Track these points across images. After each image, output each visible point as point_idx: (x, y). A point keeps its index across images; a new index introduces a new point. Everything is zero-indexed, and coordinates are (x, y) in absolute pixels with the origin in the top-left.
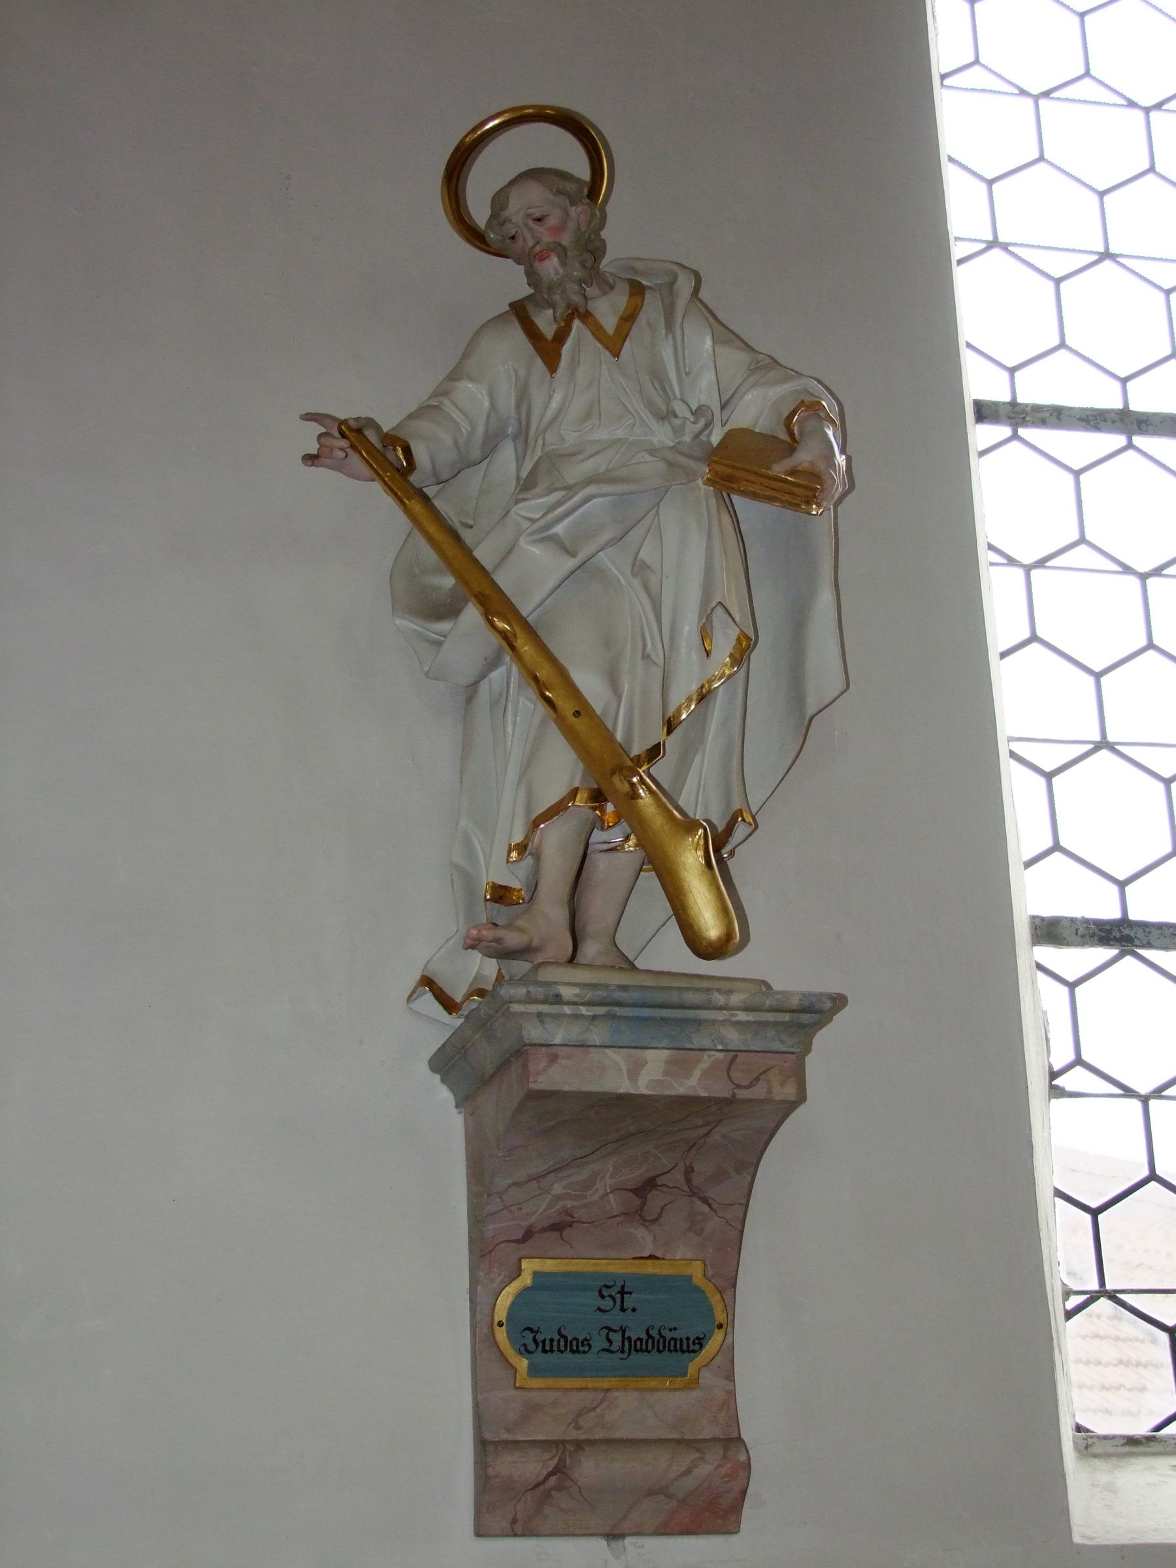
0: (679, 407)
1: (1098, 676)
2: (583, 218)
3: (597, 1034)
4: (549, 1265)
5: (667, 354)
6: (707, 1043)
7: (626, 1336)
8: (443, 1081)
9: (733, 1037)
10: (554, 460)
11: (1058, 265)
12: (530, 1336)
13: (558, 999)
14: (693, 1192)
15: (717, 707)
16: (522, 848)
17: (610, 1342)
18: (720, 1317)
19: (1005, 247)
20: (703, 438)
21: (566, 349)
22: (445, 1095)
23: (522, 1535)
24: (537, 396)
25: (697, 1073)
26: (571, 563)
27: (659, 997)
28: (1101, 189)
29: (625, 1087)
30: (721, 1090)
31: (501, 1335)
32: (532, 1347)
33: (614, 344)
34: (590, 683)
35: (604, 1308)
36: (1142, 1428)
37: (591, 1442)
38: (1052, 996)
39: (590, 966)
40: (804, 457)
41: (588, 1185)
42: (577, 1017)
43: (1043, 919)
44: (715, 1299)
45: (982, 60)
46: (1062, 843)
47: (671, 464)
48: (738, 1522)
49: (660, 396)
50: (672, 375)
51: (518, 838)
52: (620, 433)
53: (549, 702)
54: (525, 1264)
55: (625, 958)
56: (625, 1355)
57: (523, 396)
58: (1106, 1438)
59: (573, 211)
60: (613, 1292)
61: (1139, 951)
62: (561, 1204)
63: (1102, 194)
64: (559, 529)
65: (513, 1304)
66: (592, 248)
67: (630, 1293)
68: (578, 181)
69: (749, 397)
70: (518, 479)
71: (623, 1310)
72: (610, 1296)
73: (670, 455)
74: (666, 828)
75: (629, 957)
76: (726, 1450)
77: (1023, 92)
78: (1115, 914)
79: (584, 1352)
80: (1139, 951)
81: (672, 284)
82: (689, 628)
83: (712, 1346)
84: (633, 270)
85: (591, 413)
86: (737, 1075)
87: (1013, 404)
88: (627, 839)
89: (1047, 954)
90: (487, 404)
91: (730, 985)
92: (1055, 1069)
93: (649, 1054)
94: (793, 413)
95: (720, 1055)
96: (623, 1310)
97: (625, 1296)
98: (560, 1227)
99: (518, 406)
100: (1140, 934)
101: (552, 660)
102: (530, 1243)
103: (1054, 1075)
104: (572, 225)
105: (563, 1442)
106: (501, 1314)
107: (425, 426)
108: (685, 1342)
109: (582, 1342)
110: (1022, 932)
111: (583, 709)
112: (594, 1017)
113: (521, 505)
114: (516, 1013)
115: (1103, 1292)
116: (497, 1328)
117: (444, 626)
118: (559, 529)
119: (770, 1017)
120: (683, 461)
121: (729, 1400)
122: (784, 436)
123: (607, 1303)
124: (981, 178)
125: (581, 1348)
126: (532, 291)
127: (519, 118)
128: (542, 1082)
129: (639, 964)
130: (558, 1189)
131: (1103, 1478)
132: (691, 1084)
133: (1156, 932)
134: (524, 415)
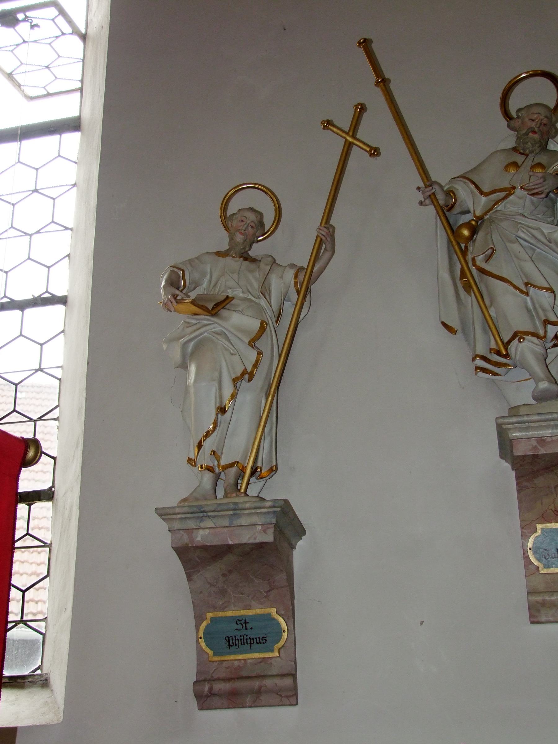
7: (236, 638)
49: (216, 307)
55: (271, 501)
60: (243, 622)
67: (248, 623)
71: (246, 629)
79: (263, 643)
97: (247, 624)
108: (258, 639)
109: (262, 639)
116: (199, 639)
123: (239, 627)
125: (261, 641)
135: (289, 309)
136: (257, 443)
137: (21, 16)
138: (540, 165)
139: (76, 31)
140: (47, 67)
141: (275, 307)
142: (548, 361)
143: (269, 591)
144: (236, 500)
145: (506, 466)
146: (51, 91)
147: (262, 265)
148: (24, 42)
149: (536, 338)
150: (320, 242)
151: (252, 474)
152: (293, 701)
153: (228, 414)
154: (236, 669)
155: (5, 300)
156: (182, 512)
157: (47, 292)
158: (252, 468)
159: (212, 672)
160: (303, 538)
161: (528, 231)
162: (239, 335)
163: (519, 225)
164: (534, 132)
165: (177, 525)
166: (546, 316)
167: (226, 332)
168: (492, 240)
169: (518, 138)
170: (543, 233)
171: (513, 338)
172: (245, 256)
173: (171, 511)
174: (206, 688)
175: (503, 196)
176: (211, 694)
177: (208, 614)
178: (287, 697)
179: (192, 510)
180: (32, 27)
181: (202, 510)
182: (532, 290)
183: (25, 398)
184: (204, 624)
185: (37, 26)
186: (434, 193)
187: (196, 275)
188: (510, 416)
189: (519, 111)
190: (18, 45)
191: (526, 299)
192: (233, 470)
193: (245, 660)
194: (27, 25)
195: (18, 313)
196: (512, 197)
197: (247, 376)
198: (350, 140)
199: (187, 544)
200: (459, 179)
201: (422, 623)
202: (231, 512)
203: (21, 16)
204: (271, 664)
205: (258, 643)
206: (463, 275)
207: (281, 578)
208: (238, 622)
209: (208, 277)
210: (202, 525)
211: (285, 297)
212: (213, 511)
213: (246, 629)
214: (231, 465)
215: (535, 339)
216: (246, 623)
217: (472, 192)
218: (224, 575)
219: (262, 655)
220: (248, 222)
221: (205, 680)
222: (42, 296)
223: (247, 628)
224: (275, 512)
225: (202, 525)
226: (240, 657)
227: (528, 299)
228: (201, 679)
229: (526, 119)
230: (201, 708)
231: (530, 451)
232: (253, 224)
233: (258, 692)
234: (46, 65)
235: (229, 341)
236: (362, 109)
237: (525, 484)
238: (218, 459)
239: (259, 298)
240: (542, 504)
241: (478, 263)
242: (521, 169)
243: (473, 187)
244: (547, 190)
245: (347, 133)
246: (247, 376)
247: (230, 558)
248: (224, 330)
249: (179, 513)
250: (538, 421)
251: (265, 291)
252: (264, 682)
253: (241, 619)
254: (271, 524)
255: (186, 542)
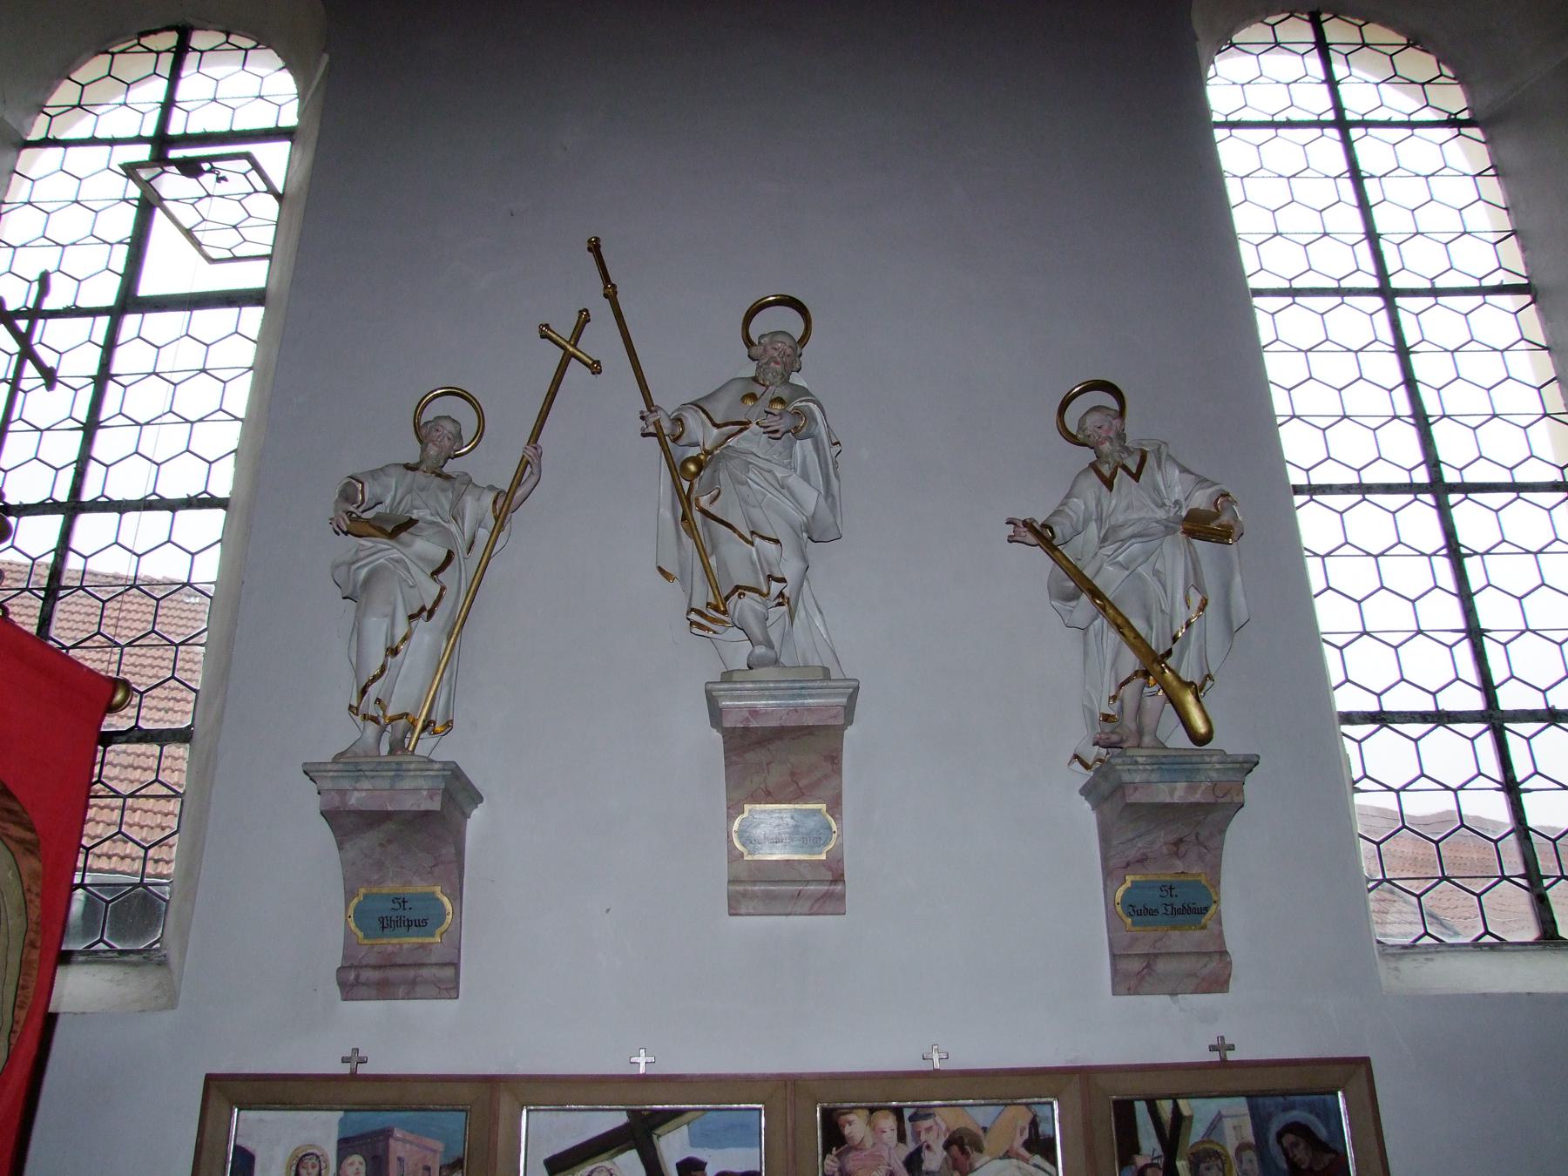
0: (1166, 501)
1: (1359, 602)
2: (1118, 425)
3: (1154, 777)
4: (1138, 878)
5: (1159, 478)
6: (1203, 779)
8: (1086, 799)
9: (1214, 775)
10: (1115, 529)
11: (1323, 423)
12: (1131, 908)
13: (1136, 763)
14: (1200, 844)
15: (1194, 630)
16: (1114, 698)
17: (1166, 910)
18: (1215, 898)
19: (1298, 417)
20: (1179, 513)
21: (1115, 481)
22: (1087, 805)
23: (1134, 994)
24: (1105, 502)
25: (1199, 792)
26: (1127, 573)
27: (1181, 760)
29: (1168, 800)
30: (1211, 799)
31: (1119, 908)
32: (1132, 913)
33: (1136, 477)
34: (1138, 624)
36: (1408, 941)
37: (1161, 954)
38: (1350, 748)
39: (1148, 748)
40: (1225, 519)
41: (1152, 843)
42: (1145, 770)
43: (1344, 713)
44: (1212, 890)
46: (1350, 678)
47: (1166, 527)
48: (1228, 988)
50: (1162, 487)
51: (1112, 694)
52: (1142, 514)
53: (1122, 633)
54: (1127, 877)
57: (1099, 502)
58: (1392, 946)
59: (1114, 422)
61: (1390, 725)
62: (1141, 851)
64: (1120, 558)
65: (1123, 895)
66: (1121, 436)
68: (1115, 410)
69: (1197, 494)
70: (1099, 537)
71: (1171, 896)
73: (1166, 523)
74: (1179, 686)
76: (1221, 956)
77: (1300, 350)
78: (1376, 708)
80: (1390, 725)
81: (1159, 449)
82: (1180, 596)
83: (1213, 908)
84: (1140, 444)
85: (1129, 507)
86: (1218, 793)
87: (1310, 485)
88: (1159, 690)
89: (1346, 729)
90: (1083, 507)
91: (1212, 753)
92: (1355, 779)
93: (1178, 785)
94: (1217, 500)
95: (1209, 784)
96: (1171, 896)
98: (1142, 860)
99: (1097, 505)
100: (1390, 717)
101: (1121, 615)
102: (1129, 868)
103: (1355, 782)
104: (1114, 428)
105: (1148, 954)
106: (1118, 899)
107: (1056, 519)
110: (1336, 718)
111: (1138, 636)
112: (1153, 770)
113: (1103, 549)
114: (1119, 770)
115: (1385, 880)
117: (1073, 603)
118: (1120, 558)
119: (1231, 766)
120: (1171, 525)
121: (1220, 935)
122: (1214, 510)
123: (397, 906)
124: (1285, 389)
128: (1132, 799)
129: (1168, 745)
130: (1140, 845)
131: (1393, 965)
132: (1197, 797)
133: (1397, 716)
134: (1099, 510)
135: (483, 535)
136: (432, 693)
137: (206, 166)
138: (780, 400)
139: (271, 190)
140: (235, 227)
141: (467, 536)
142: (769, 623)
143: (434, 866)
144: (401, 759)
145: (717, 736)
146: (238, 255)
147: (457, 484)
148: (209, 195)
149: (757, 595)
150: (524, 464)
151: (424, 729)
152: (453, 993)
153: (400, 656)
154: (389, 955)
155: (154, 497)
156: (335, 769)
157: (205, 492)
158: (424, 721)
159: (360, 957)
160: (479, 805)
161: (761, 474)
162: (420, 564)
163: (751, 466)
164: (777, 363)
165: (327, 784)
166: (770, 571)
167: (406, 560)
169: (759, 368)
170: (776, 477)
171: (733, 593)
172: (438, 471)
173: (322, 768)
174: (352, 976)
175: (737, 430)
176: (357, 982)
178: (446, 989)
179: (346, 768)
180: (219, 179)
181: (359, 768)
182: (757, 541)
183: (200, 604)
184: (355, 901)
185: (224, 179)
186: (659, 420)
187: (378, 490)
188: (721, 682)
189: (762, 337)
190: (200, 198)
191: (751, 551)
192: (403, 722)
193: (400, 944)
194: (213, 176)
195: (167, 514)
196: (745, 433)
197: (425, 614)
198: (571, 349)
199: (338, 808)
200: (690, 406)
201: (608, 910)
202: (392, 773)
203: (206, 166)
204: (431, 950)
206: (684, 518)
207: (448, 851)
208: (395, 901)
209: (392, 493)
210: (358, 785)
211: (480, 523)
212: (372, 771)
213: (404, 909)
214: (401, 717)
215: (756, 596)
216: (404, 902)
217: (703, 422)
218: (381, 845)
219: (420, 940)
220: (445, 432)
221: (351, 967)
222: (200, 497)
224: (444, 776)
225: (358, 785)
226: (395, 941)
227: (754, 549)
228: (346, 965)
229: (769, 347)
230: (345, 999)
231: (741, 722)
232: (450, 436)
233: (414, 983)
234: (234, 224)
235: (408, 570)
236: (584, 319)
237: (734, 758)
238: (384, 709)
239: (448, 522)
240: (751, 782)
241: (702, 504)
242: (760, 402)
243: (704, 416)
244: (784, 430)
245: (568, 342)
246: (425, 614)
247: (391, 826)
248: (404, 558)
249: (330, 771)
251: (457, 516)
252: (421, 971)
253: (398, 897)
254: (439, 789)
255: (337, 804)
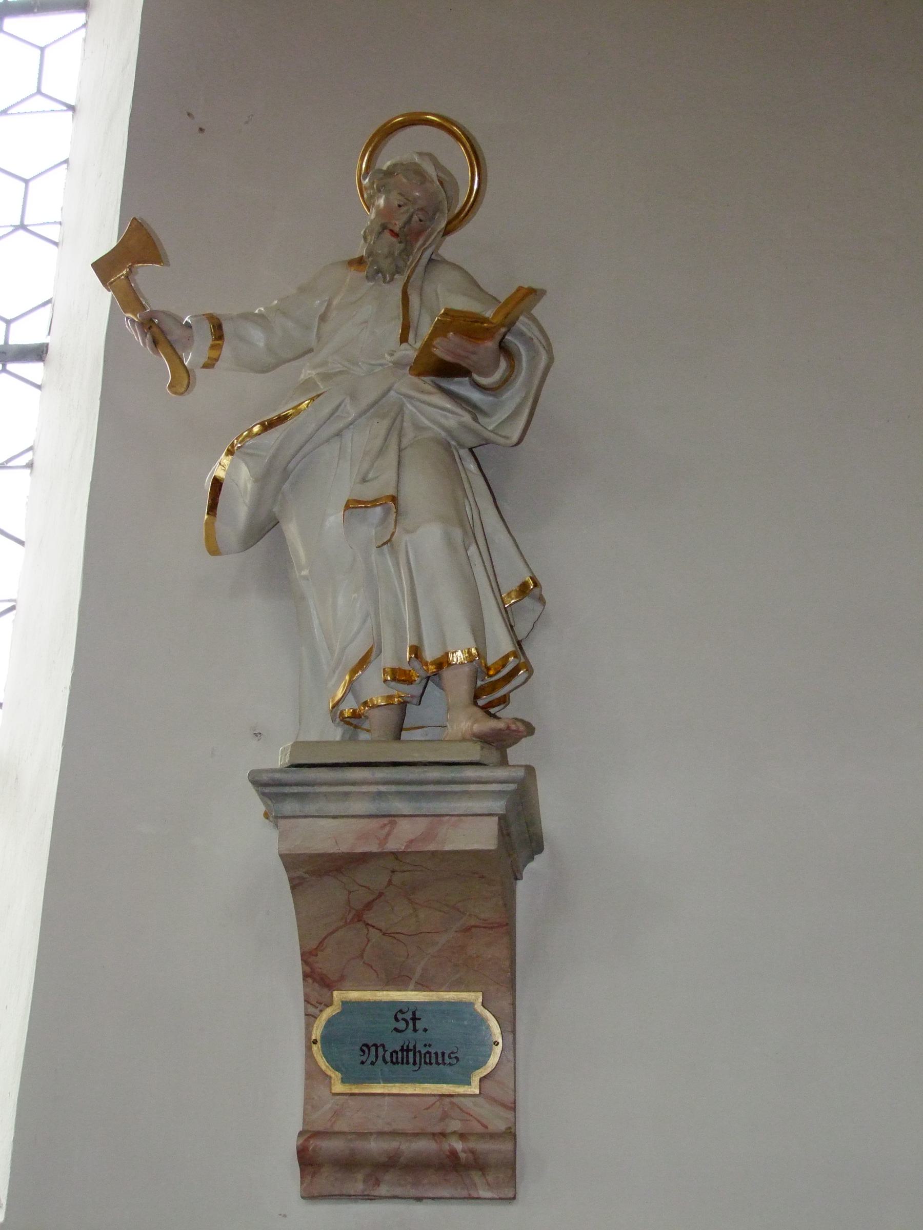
28: (35, 90)
35: (400, 1029)
45: (27, 177)
56: (416, 1068)
60: (409, 1016)
63: (39, 92)
67: (419, 1019)
71: (415, 1030)
72: (403, 1019)
75: (405, 723)
79: (450, 1064)
96: (415, 1030)
97: (417, 1021)
123: (402, 1025)
125: (447, 1060)
126: (460, 651)
127: (445, 125)
168: (472, 491)
177: (480, 995)
205: (394, 1064)
219: (445, 1088)
223: (417, 1029)
230: (310, 1196)
250: (330, 784)
